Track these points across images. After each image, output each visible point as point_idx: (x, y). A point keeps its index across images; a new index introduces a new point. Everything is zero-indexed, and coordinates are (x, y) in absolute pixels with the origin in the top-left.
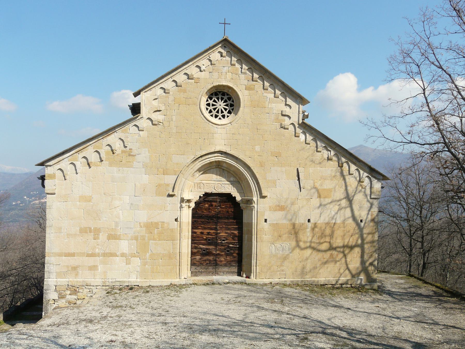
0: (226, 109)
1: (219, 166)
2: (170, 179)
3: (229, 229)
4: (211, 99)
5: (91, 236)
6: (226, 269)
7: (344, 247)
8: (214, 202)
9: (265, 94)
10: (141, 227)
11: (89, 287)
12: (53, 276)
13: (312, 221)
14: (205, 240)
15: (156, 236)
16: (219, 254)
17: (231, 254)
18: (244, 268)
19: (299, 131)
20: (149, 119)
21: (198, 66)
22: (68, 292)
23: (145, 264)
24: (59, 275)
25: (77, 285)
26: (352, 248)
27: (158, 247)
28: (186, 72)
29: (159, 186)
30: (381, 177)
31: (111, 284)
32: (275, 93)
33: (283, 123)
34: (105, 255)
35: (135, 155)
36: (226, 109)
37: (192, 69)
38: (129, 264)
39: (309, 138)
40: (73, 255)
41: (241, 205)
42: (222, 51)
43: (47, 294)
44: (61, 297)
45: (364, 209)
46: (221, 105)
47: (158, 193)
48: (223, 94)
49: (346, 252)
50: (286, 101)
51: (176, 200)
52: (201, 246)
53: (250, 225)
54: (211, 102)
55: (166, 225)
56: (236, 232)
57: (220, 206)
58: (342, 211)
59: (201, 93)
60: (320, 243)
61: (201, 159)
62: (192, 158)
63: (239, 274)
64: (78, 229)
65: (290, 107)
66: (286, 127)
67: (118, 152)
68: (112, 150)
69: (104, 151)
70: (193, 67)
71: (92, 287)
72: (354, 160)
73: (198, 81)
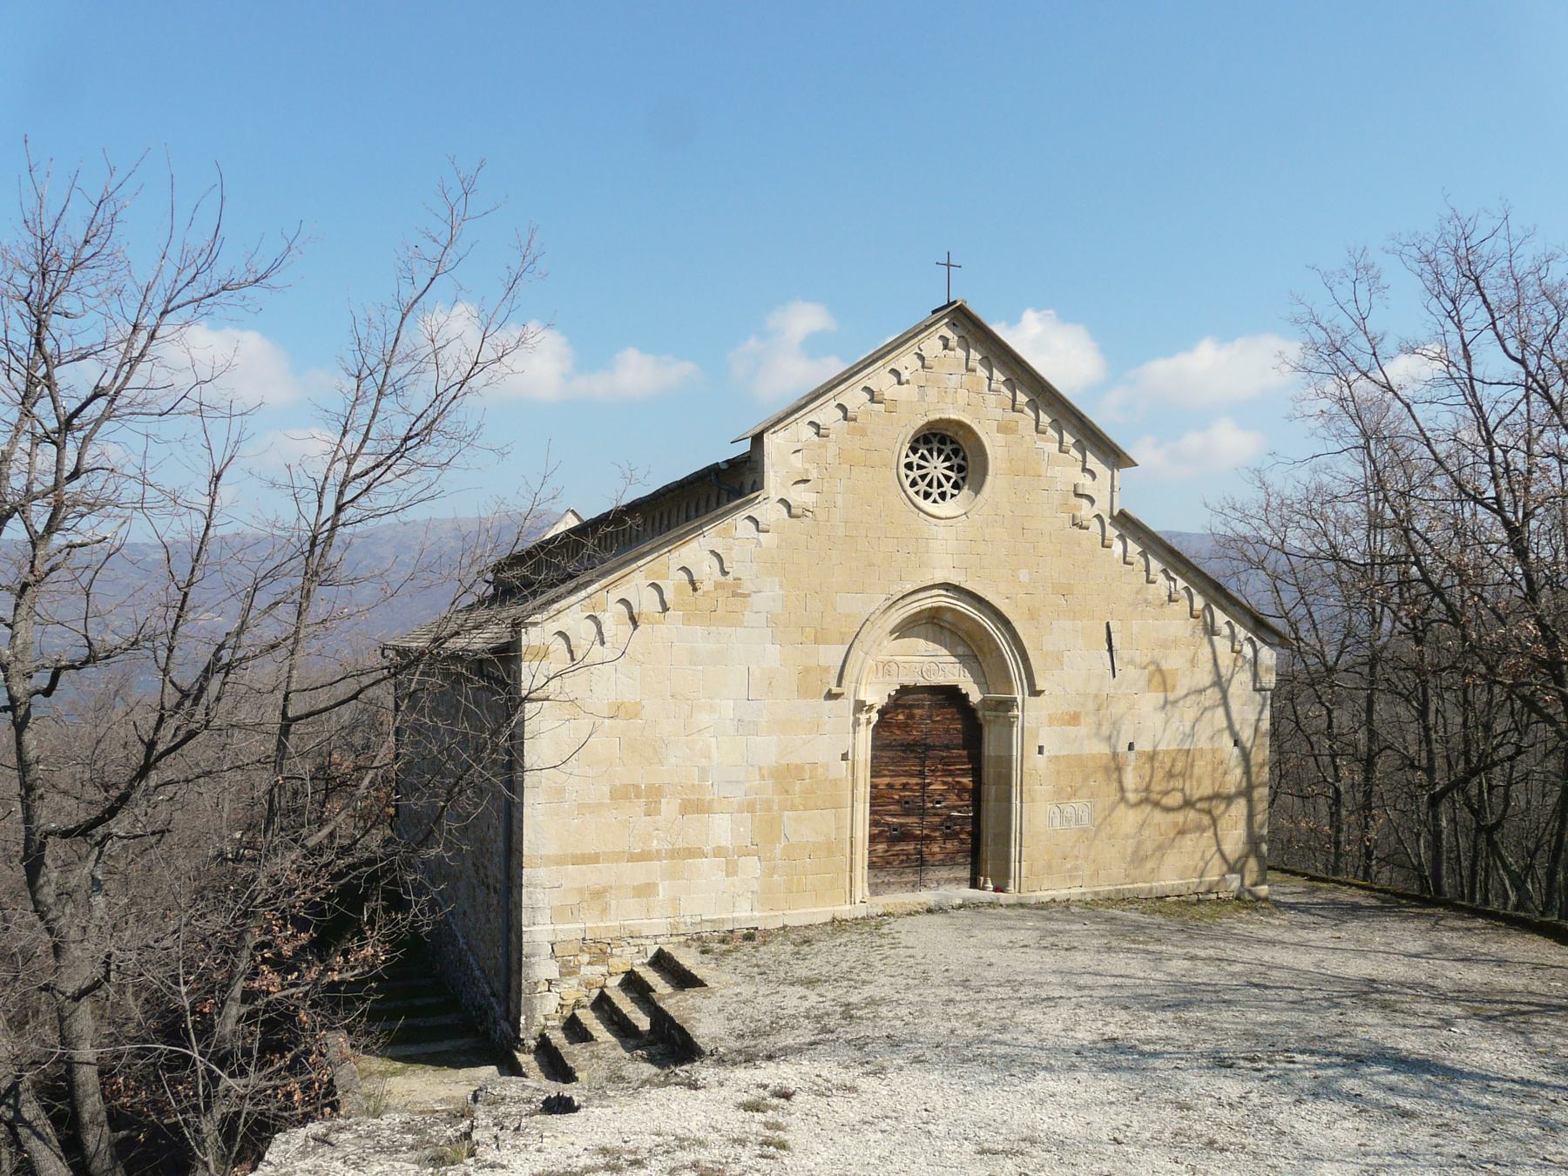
0: (948, 478)
1: (957, 622)
2: (832, 655)
3: (951, 773)
4: (914, 450)
5: (639, 806)
6: (944, 873)
7: (1210, 798)
8: (918, 707)
9: (1040, 444)
10: (763, 778)
11: (638, 941)
12: (543, 917)
13: (1136, 747)
14: (898, 802)
15: (797, 801)
16: (928, 836)
17: (955, 835)
18: (989, 867)
19: (1112, 532)
20: (782, 501)
21: (894, 372)
22: (585, 958)
23: (771, 871)
24: (558, 914)
25: (605, 936)
26: (1229, 799)
27: (809, 827)
28: (868, 383)
29: (806, 671)
30: (1277, 640)
31: (691, 930)
32: (1061, 442)
33: (1078, 514)
34: (674, 854)
35: (749, 595)
36: (948, 478)
37: (879, 378)
38: (735, 873)
39: (1134, 549)
40: (594, 859)
41: (980, 714)
42: (949, 334)
43: (531, 966)
44: (568, 971)
45: (1250, 711)
46: (937, 467)
47: (803, 692)
48: (943, 440)
49: (1217, 812)
50: (1084, 462)
51: (846, 705)
52: (889, 819)
53: (1006, 762)
54: (915, 459)
55: (820, 770)
56: (966, 780)
57: (930, 717)
58: (1208, 714)
59: (900, 440)
60: (1166, 793)
61: (902, 603)
62: (880, 601)
63: (974, 884)
64: (606, 789)
65: (1094, 476)
66: (1085, 523)
67: (706, 586)
68: (692, 582)
69: (673, 583)
70: (885, 373)
71: (643, 941)
72: (1224, 602)
73: (892, 406)
